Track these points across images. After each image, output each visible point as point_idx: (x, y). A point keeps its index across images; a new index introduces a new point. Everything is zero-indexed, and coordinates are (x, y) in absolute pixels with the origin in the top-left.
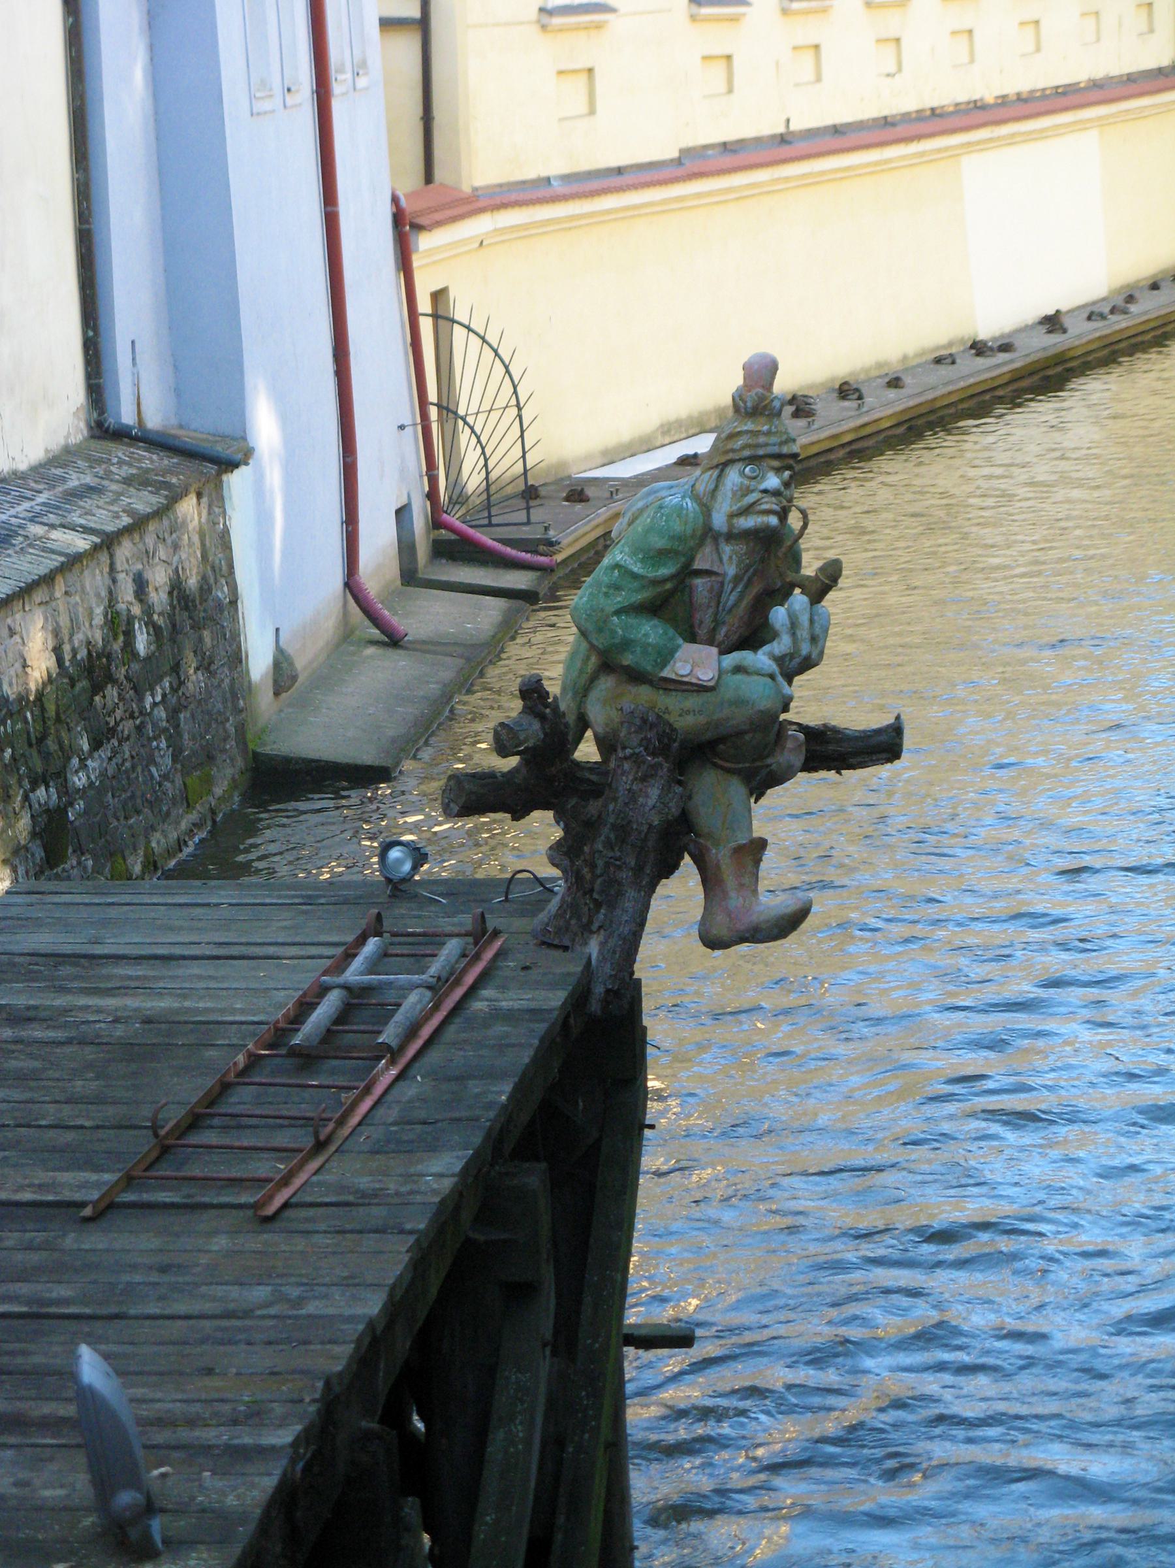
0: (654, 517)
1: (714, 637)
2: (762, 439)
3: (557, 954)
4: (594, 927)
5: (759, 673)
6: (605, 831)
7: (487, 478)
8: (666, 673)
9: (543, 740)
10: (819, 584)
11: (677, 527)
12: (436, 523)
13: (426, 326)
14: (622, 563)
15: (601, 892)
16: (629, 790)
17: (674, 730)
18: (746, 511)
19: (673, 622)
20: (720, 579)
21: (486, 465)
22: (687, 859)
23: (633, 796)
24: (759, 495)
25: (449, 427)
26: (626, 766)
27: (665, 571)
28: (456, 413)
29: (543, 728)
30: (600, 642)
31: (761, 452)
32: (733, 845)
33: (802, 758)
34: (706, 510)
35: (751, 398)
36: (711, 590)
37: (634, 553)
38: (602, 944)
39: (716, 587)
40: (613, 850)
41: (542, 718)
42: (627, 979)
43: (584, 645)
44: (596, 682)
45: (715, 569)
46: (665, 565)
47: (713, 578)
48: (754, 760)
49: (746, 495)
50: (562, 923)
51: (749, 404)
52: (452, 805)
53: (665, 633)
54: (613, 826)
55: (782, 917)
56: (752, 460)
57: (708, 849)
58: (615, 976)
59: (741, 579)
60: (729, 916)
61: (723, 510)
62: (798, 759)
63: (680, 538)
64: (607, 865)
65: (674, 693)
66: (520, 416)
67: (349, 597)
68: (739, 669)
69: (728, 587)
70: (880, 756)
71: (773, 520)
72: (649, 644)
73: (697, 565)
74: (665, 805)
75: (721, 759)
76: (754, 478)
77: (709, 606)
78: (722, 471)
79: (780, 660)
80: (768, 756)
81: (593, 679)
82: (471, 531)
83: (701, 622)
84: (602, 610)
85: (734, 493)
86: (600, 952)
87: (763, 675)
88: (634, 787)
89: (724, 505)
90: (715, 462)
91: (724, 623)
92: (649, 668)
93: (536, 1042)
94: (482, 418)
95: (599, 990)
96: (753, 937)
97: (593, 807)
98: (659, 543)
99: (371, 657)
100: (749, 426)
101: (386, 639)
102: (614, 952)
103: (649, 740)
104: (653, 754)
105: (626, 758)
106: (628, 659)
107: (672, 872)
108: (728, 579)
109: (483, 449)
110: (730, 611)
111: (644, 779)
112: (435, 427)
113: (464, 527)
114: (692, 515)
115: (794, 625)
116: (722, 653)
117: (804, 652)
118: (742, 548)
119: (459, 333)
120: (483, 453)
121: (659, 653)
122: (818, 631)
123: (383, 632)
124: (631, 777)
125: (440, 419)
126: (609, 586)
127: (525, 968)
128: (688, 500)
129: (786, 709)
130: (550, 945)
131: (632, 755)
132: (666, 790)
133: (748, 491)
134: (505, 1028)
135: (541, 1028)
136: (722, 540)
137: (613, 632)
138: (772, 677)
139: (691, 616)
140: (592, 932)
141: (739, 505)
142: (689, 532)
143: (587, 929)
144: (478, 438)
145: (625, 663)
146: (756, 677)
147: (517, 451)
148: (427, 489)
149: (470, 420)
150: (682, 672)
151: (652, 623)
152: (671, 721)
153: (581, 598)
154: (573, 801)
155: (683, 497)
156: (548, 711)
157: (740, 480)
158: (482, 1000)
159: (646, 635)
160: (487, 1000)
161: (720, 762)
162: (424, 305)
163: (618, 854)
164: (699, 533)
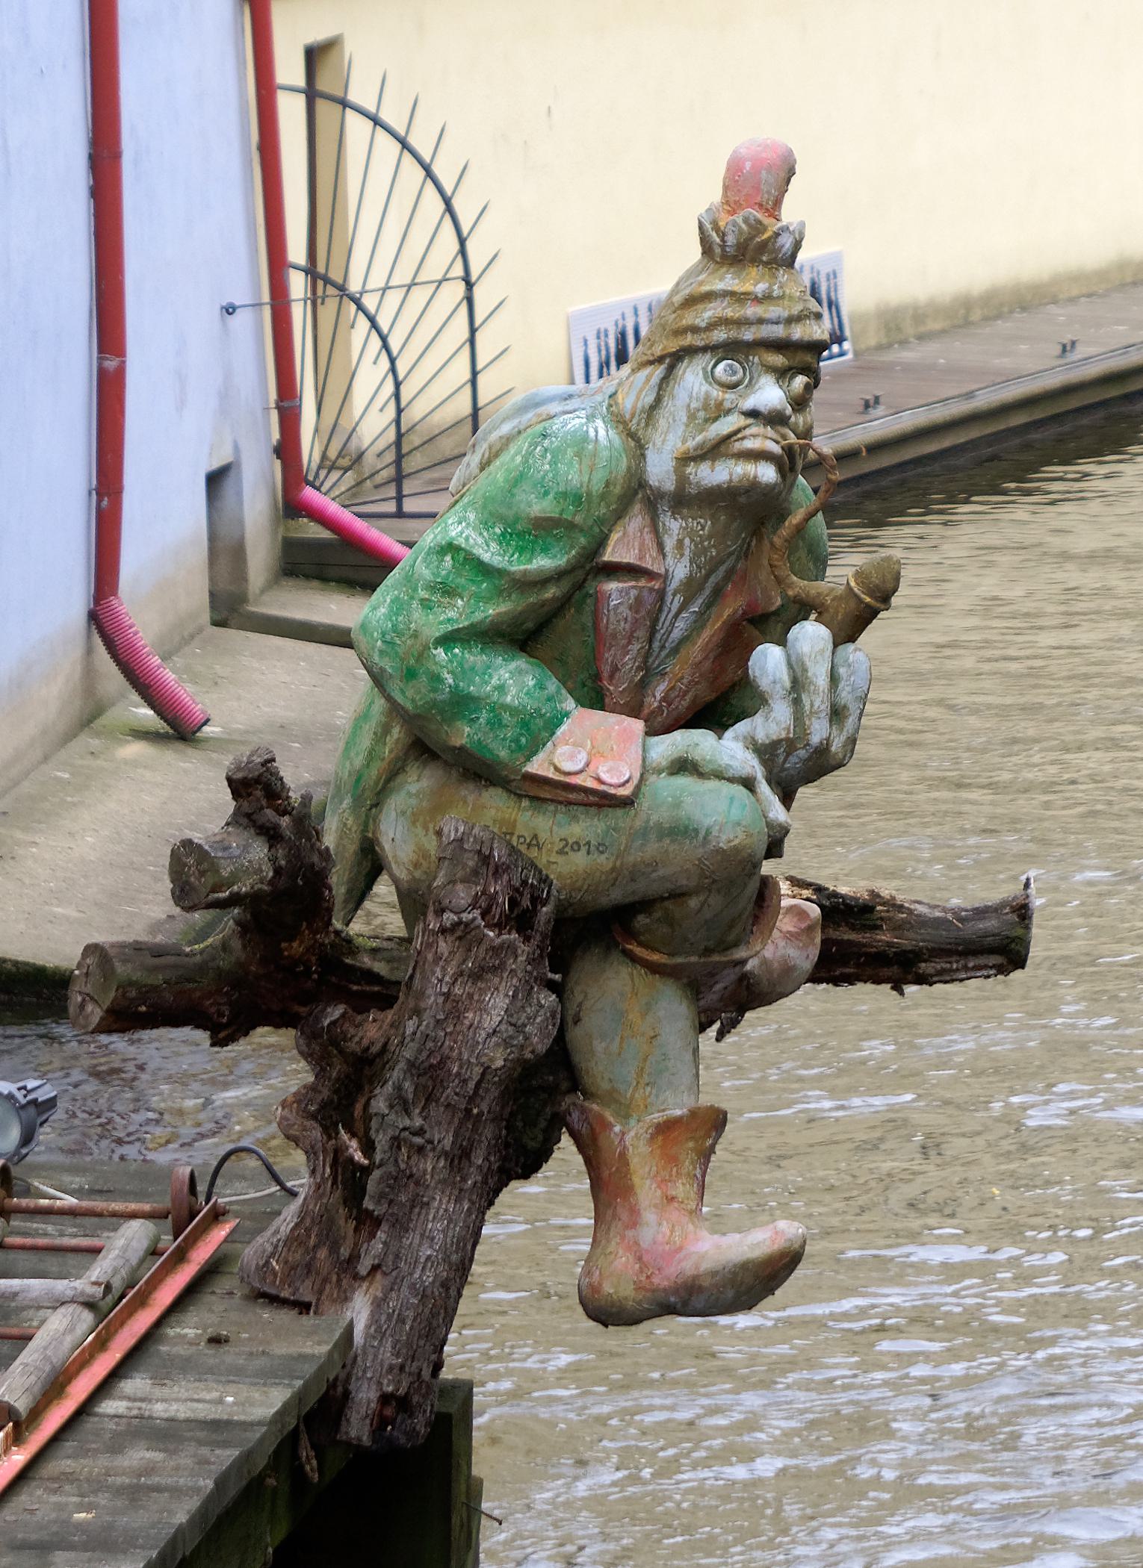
0: (530, 453)
1: (641, 704)
2: (751, 311)
3: (285, 1317)
4: (363, 1268)
5: (719, 775)
6: (396, 1074)
7: (398, 421)
8: (537, 766)
9: (271, 883)
10: (852, 604)
11: (574, 475)
12: (292, 507)
13: (291, 111)
14: (461, 542)
15: (380, 1197)
16: (447, 996)
17: (545, 880)
18: (715, 450)
19: (557, 665)
20: (656, 585)
21: (397, 395)
22: (566, 1141)
23: (454, 1008)
24: (742, 421)
25: (327, 312)
26: (443, 946)
27: (542, 563)
28: (342, 288)
29: (273, 860)
30: (408, 696)
31: (748, 335)
32: (657, 1117)
33: (814, 952)
34: (637, 444)
35: (735, 224)
36: (637, 605)
37: (486, 524)
38: (378, 1304)
39: (649, 599)
40: (407, 1112)
41: (271, 835)
42: (426, 1374)
43: (380, 703)
44: (400, 779)
45: (648, 564)
46: (545, 550)
47: (642, 583)
48: (708, 951)
49: (716, 419)
50: (297, 1256)
51: (731, 240)
52: (90, 1007)
53: (541, 686)
54: (411, 1064)
55: (745, 1266)
56: (732, 349)
57: (608, 1126)
58: (402, 1368)
59: (701, 588)
60: (640, 1259)
61: (668, 447)
62: (806, 957)
63: (578, 499)
64: (396, 1142)
65: (552, 808)
66: (469, 300)
67: (98, 641)
68: (683, 766)
69: (674, 602)
70: (981, 960)
71: (767, 473)
72: (506, 707)
73: (609, 556)
74: (519, 1028)
75: (640, 944)
76: (733, 386)
77: (630, 638)
78: (671, 368)
79: (766, 752)
80: (736, 944)
81: (393, 773)
82: (360, 525)
83: (615, 669)
84: (415, 635)
85: (692, 416)
86: (374, 1319)
87: (731, 780)
88: (457, 990)
89: (671, 436)
90: (658, 350)
91: (663, 674)
92: (503, 754)
93: (210, 1484)
94: (394, 298)
95: (365, 1395)
96: (685, 1303)
97: (372, 1029)
98: (540, 507)
99: (135, 763)
100: (728, 281)
101: (171, 731)
102: (402, 1320)
103: (493, 898)
104: (499, 926)
105: (443, 931)
106: (463, 734)
107: (536, 1168)
108: (674, 584)
109: (393, 361)
110: (675, 650)
111: (478, 975)
112: (299, 314)
113: (346, 516)
114: (606, 454)
115: (798, 684)
116: (651, 732)
117: (815, 739)
118: (704, 525)
119: (357, 127)
120: (393, 370)
121: (525, 724)
122: (845, 695)
123: (159, 713)
124: (450, 971)
125: (315, 301)
126: (432, 588)
127: (216, 1341)
128: (599, 423)
129: (774, 849)
130: (274, 1300)
131: (456, 925)
132: (523, 995)
133: (720, 411)
134: (149, 1455)
135: (227, 1456)
136: (663, 507)
137: (436, 678)
138: (748, 784)
139: (596, 656)
140: (356, 1277)
141: (699, 438)
142: (597, 487)
143: (348, 1273)
144: (384, 339)
145: (457, 741)
146: (713, 784)
147: (460, 370)
148: (276, 436)
149: (370, 302)
150: (568, 766)
151: (513, 665)
152: (542, 862)
153: (375, 608)
154: (336, 1012)
155: (591, 418)
156: (285, 821)
157: (705, 387)
158: (122, 1398)
159: (501, 688)
160: (129, 1399)
161: (639, 951)
162: (289, 69)
163: (418, 1122)
164: (617, 490)
